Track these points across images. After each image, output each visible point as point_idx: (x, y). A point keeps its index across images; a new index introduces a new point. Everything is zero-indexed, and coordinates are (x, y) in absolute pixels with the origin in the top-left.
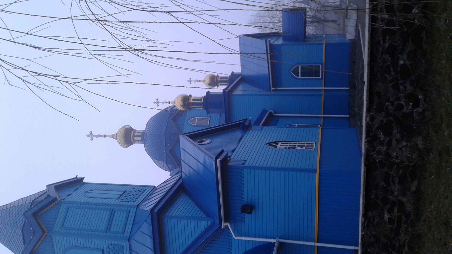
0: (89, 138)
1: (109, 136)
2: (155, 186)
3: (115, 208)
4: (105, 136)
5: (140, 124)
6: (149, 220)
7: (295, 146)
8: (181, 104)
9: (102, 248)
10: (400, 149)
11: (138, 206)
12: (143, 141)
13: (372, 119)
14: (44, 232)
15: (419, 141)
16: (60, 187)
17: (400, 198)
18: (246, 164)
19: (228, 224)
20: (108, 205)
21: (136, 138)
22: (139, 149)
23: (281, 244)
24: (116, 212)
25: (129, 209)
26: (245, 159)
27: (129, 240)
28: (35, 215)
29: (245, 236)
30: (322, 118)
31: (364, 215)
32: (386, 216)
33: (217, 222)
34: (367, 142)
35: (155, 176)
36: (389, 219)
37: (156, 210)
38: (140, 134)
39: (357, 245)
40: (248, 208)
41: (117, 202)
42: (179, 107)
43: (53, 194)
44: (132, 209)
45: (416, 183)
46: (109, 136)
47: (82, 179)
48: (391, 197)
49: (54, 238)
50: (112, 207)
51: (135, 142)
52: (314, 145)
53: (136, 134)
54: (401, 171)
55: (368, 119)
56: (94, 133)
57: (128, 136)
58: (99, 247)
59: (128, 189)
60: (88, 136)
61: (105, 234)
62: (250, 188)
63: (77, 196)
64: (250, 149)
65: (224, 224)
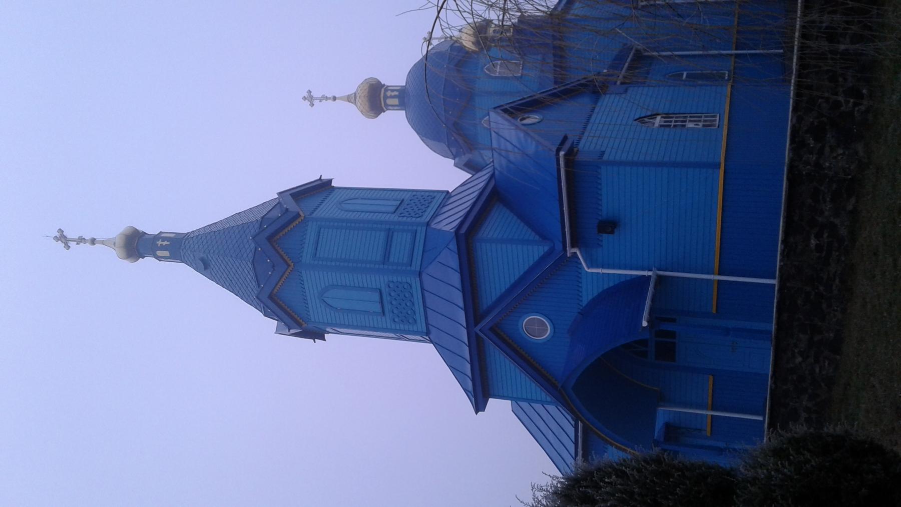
0: (307, 103)
1: (341, 98)
2: (448, 192)
3: (392, 227)
4: (93, 241)
5: (396, 76)
6: (453, 246)
7: (685, 121)
8: (473, 39)
9: (379, 287)
10: (835, 158)
11: (428, 224)
12: (402, 105)
13: (800, 120)
14: (289, 266)
15: (860, 147)
16: (301, 194)
17: (832, 219)
18: (605, 157)
19: (574, 250)
20: (381, 223)
21: (390, 101)
22: (396, 121)
23: (660, 279)
24: (395, 234)
25: (415, 228)
26: (603, 149)
27: (420, 274)
28: (270, 239)
29: (603, 268)
30: (733, 59)
31: (784, 242)
32: (813, 242)
33: (559, 246)
34: (792, 150)
35: (440, 173)
36: (817, 245)
37: (463, 231)
38: (396, 93)
39: (774, 278)
40: (609, 226)
41: (395, 218)
42: (468, 42)
43: (292, 205)
44: (419, 228)
45: (853, 200)
46: (341, 98)
47: (330, 181)
48: (820, 219)
49: (303, 272)
50: (388, 227)
51: (388, 107)
52: (718, 118)
53: (389, 93)
54: (834, 186)
55: (794, 120)
56: (315, 94)
57: (375, 98)
58: (374, 287)
59: (407, 197)
60: (305, 98)
61: (381, 266)
62: (613, 195)
63: (327, 209)
64: (612, 127)
65: (570, 251)
